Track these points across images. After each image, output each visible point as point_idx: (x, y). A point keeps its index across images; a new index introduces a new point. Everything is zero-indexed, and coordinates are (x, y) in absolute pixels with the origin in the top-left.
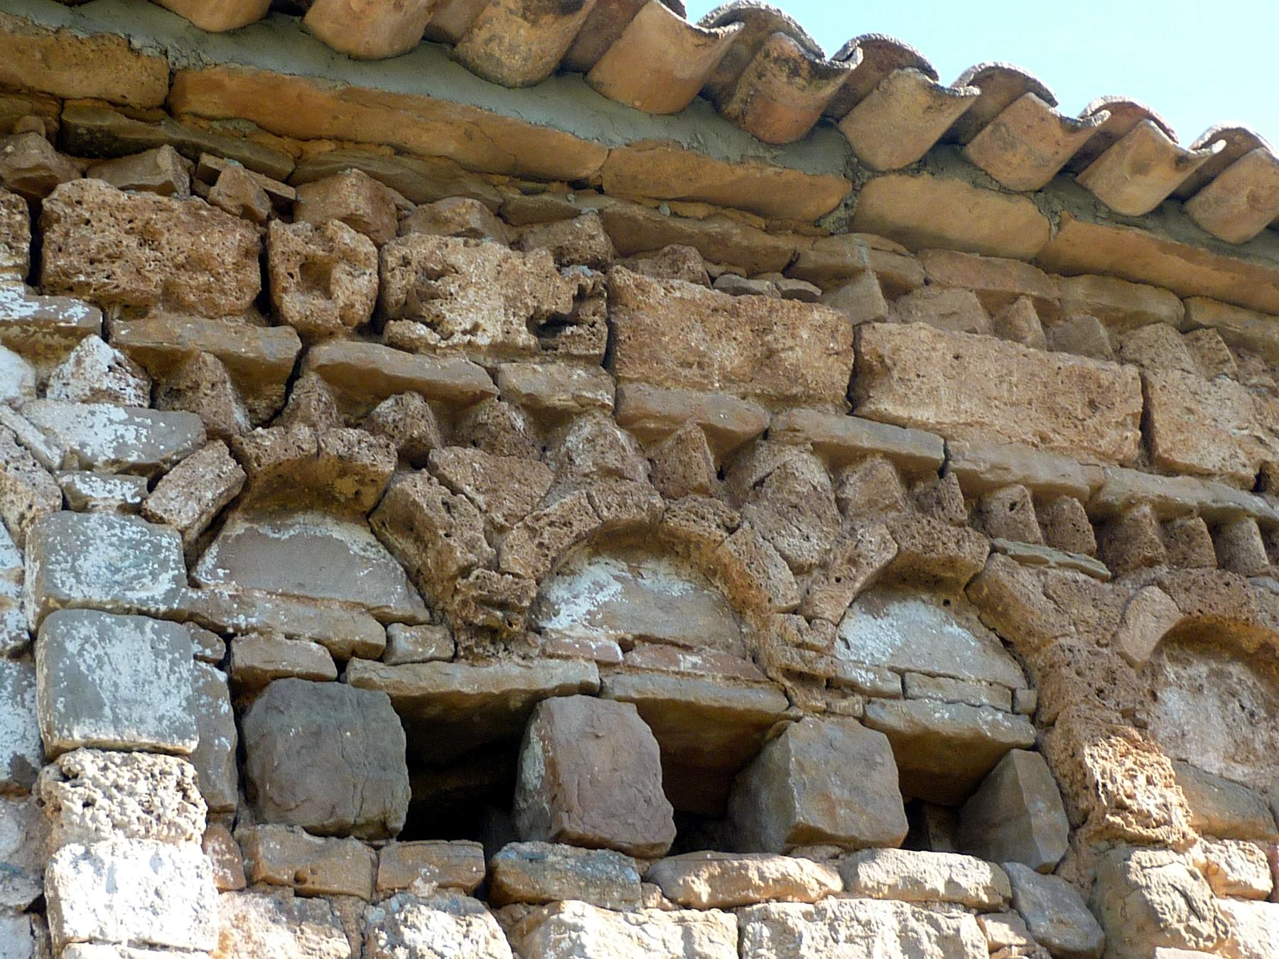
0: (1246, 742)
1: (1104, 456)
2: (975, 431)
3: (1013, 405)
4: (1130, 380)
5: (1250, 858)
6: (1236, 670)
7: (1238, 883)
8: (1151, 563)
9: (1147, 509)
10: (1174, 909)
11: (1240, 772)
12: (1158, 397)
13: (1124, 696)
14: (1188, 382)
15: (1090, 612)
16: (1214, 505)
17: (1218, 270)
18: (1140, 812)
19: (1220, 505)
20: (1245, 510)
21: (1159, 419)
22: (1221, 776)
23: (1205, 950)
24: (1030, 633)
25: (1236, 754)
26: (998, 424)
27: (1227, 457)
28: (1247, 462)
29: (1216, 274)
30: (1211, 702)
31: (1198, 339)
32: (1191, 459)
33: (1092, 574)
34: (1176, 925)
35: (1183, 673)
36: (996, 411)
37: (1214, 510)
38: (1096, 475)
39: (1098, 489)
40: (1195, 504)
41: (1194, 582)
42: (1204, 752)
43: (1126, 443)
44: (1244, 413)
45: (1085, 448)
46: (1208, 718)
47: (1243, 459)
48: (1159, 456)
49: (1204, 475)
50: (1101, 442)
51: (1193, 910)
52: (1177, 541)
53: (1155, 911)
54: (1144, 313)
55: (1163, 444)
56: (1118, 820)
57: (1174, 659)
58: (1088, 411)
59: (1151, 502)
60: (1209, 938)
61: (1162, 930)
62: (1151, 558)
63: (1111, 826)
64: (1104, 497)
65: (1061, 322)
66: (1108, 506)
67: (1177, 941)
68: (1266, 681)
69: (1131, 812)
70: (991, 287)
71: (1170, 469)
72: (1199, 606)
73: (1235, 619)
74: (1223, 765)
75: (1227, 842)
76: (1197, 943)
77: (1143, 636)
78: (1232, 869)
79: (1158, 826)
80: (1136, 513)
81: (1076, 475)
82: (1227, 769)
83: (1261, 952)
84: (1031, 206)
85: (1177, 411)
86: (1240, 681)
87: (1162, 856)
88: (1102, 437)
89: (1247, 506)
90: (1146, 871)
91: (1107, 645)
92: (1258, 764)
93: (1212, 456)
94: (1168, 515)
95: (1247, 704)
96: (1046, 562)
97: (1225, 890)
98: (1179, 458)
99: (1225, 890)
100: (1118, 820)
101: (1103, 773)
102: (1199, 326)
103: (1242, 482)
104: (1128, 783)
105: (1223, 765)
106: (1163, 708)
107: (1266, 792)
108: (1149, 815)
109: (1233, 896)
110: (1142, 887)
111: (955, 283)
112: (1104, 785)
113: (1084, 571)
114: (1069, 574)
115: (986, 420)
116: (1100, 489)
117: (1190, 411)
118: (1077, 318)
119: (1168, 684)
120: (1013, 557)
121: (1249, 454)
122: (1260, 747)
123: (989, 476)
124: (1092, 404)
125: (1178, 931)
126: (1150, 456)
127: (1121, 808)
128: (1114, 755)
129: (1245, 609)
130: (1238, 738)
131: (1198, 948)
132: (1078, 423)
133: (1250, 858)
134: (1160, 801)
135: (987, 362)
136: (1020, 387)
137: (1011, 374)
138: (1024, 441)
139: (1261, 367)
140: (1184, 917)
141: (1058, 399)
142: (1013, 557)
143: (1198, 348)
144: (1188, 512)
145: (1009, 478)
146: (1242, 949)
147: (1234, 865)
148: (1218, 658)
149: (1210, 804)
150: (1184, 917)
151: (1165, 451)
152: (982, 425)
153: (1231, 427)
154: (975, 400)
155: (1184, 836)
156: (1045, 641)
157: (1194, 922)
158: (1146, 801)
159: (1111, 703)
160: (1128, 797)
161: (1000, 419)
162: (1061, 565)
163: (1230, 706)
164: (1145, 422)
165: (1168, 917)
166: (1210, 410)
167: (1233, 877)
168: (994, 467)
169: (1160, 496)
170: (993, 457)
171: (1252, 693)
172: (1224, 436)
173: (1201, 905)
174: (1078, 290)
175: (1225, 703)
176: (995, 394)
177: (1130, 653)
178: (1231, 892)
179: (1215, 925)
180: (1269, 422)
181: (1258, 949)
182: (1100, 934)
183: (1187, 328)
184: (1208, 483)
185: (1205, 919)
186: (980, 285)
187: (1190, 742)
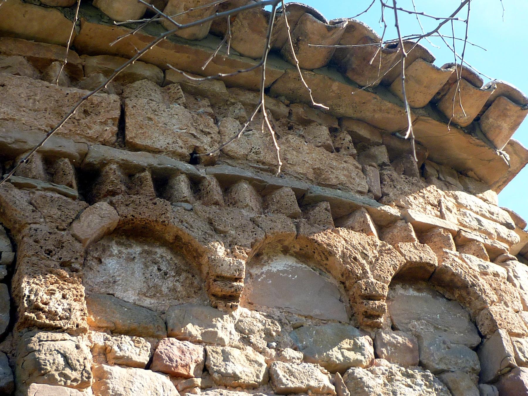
0: (155, 286)
1: (91, 139)
2: (10, 124)
3: (35, 111)
4: (112, 101)
5: (137, 345)
6: (160, 251)
7: (122, 357)
8: (113, 193)
9: (114, 166)
10: (54, 363)
11: (147, 302)
12: (129, 111)
13: (65, 255)
14: (151, 105)
15: (55, 212)
16: (159, 166)
17: (178, 52)
18: (50, 312)
19: (162, 166)
20: (178, 170)
21: (129, 122)
22: (135, 303)
23: (71, 387)
24: (15, 223)
25: (147, 292)
26: (24, 120)
27: (170, 143)
28: (183, 146)
29: (178, 55)
30: (138, 266)
31: (169, 89)
32: (148, 142)
33: (66, 195)
34: (53, 372)
35: (124, 251)
36: (23, 113)
37: (159, 169)
38: (83, 148)
39: (84, 155)
40: (146, 165)
41: (133, 202)
42: (126, 291)
43: (106, 132)
44: (185, 122)
45: (78, 134)
46: (133, 273)
47: (181, 143)
48: (127, 141)
49: (156, 152)
50: (89, 131)
51: (68, 364)
52: (136, 185)
53: (40, 364)
54: (135, 74)
55: (130, 135)
56: (33, 315)
57: (118, 243)
58: (83, 115)
59: (117, 163)
60: (75, 380)
61: (43, 375)
62: (111, 191)
63: (27, 318)
64: (88, 160)
65: (85, 78)
66: (90, 164)
67: (52, 381)
68: (180, 258)
69: (44, 312)
70: (37, 56)
71: (135, 148)
72: (132, 213)
73: (156, 221)
74: (137, 298)
75: (141, 338)
76: (65, 383)
77: (89, 226)
78: (121, 350)
79: (60, 320)
80: (107, 168)
81: (70, 147)
82: (139, 300)
83: (123, 393)
84: (59, 14)
85: (141, 118)
86: (162, 257)
87: (59, 336)
88: (90, 129)
89: (180, 168)
90: (41, 343)
91: (64, 230)
92: (162, 299)
93: (161, 141)
94: (131, 172)
95: (164, 268)
96: (35, 187)
97: (114, 361)
98: (138, 141)
99: (114, 361)
100: (33, 315)
101: (31, 291)
102: (171, 82)
103: (182, 157)
104: (46, 297)
105: (137, 298)
106: (103, 267)
107: (164, 313)
108: (56, 314)
109: (120, 365)
110: (35, 351)
111: (14, 53)
112: (29, 297)
113: (60, 193)
114: (49, 194)
115: (16, 117)
116: (86, 154)
117: (150, 119)
118: (92, 75)
119: (111, 255)
120: (12, 183)
121: (185, 142)
122: (165, 290)
123: (15, 146)
124: (86, 112)
125: (53, 375)
126: (122, 140)
127: (37, 309)
128: (46, 283)
129: (163, 216)
130: (151, 285)
131: (65, 385)
132: (75, 121)
133: (137, 345)
134: (66, 306)
135: (21, 88)
136: (41, 102)
137: (36, 95)
138: (39, 129)
139: (207, 104)
140: (61, 368)
141: (63, 109)
142: (12, 183)
143: (168, 93)
144: (143, 170)
145: (27, 147)
146: (110, 391)
147: (123, 348)
148: (149, 244)
149: (118, 315)
150: (61, 368)
151: (131, 138)
152: (14, 120)
153: (175, 129)
154: (10, 107)
155: (77, 326)
156: (23, 226)
157: (68, 371)
158: (56, 305)
159: (55, 258)
160: (44, 304)
161: (25, 118)
162: (45, 189)
163: (151, 268)
164: (122, 123)
165: (49, 368)
166: (163, 119)
167: (119, 353)
168: (17, 141)
169: (123, 160)
170: (17, 135)
171: (169, 263)
172: (170, 132)
173: (75, 362)
174: (94, 61)
175: (147, 267)
176: (24, 104)
177: (78, 234)
178: (119, 362)
179: (82, 374)
180: (201, 127)
181: (121, 391)
182: (10, 379)
183: (163, 84)
184: (156, 155)
185: (76, 370)
186: (30, 54)
187: (118, 285)
